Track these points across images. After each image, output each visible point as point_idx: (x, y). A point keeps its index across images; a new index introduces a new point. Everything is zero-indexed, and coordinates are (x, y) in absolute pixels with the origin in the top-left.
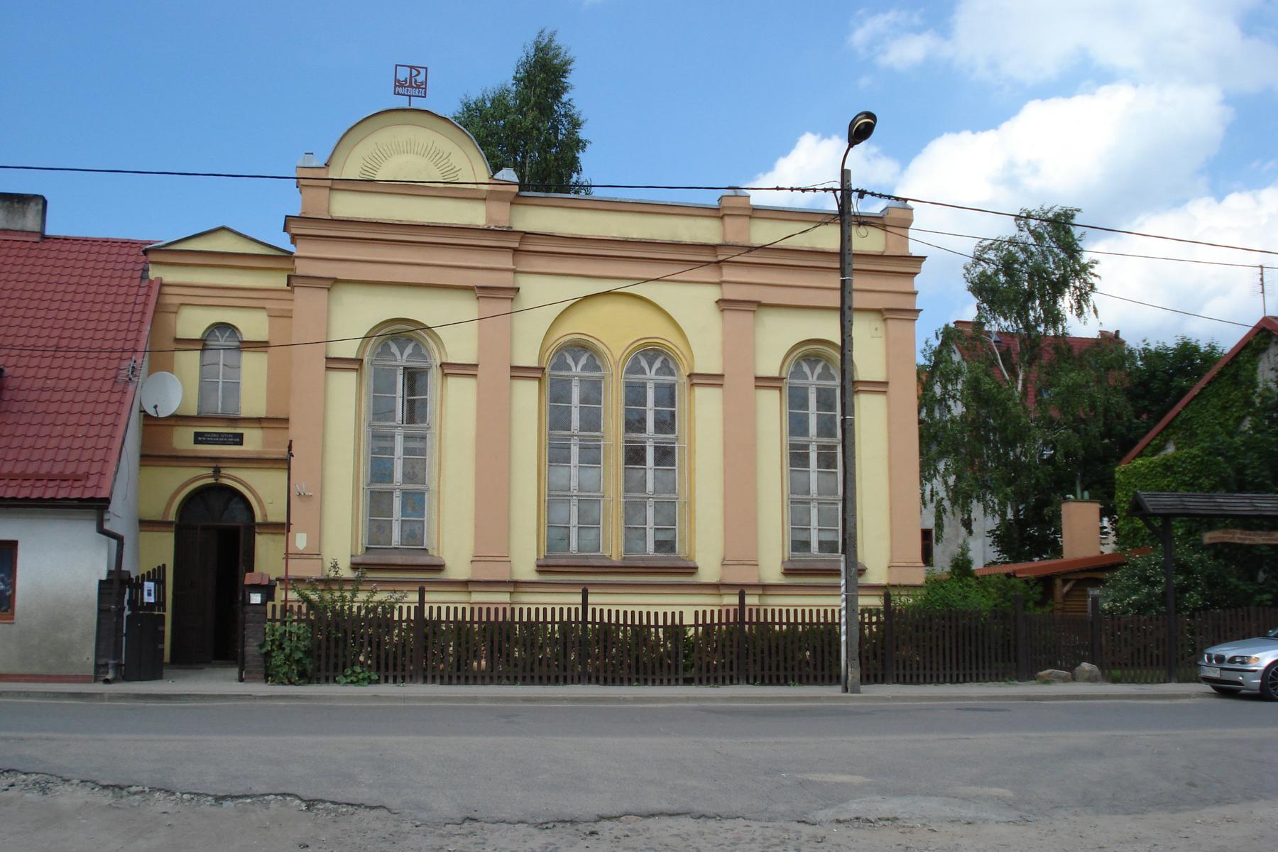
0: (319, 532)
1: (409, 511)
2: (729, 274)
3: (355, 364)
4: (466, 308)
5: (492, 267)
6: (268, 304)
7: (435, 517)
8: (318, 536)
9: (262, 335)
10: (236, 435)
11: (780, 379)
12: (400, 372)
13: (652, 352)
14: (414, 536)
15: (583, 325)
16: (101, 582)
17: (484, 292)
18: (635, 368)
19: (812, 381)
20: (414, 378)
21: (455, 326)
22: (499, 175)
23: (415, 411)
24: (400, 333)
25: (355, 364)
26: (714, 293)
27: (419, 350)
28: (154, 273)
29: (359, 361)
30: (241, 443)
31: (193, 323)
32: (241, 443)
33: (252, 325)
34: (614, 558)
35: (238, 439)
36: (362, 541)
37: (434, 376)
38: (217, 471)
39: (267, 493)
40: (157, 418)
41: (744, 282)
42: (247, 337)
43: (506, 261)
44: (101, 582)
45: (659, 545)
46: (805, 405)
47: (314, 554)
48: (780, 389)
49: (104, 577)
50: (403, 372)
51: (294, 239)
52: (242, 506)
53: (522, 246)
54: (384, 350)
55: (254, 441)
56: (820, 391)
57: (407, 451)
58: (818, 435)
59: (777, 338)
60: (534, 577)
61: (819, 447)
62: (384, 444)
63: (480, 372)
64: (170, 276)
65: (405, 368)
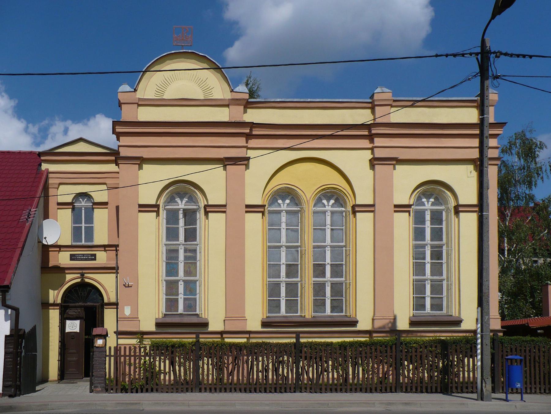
0: (140, 303)
1: (188, 293)
2: (378, 142)
3: (154, 208)
4: (218, 171)
5: (232, 146)
6: (107, 181)
7: (411, 251)
8: (135, 309)
9: (105, 200)
10: (92, 255)
11: (409, 206)
12: (181, 212)
13: (330, 194)
14: (191, 305)
15: (284, 179)
16: (6, 336)
17: (226, 162)
18: (318, 201)
19: (428, 205)
20: (190, 216)
21: (213, 182)
22: (237, 89)
23: (191, 235)
24: (182, 189)
25: (154, 208)
26: (368, 155)
27: (192, 199)
28: (44, 166)
29: (157, 206)
30: (95, 259)
31: (65, 193)
32: (95, 259)
33: (100, 194)
34: (307, 317)
35: (93, 257)
36: (163, 309)
37: (201, 215)
38: (82, 275)
39: (106, 283)
40: (48, 245)
41: (386, 146)
42: (97, 200)
43: (241, 141)
44: (6, 336)
45: (433, 307)
46: (423, 222)
47: (134, 318)
48: (409, 212)
49: (8, 333)
50: (183, 208)
51: (119, 135)
52: (97, 294)
53: (250, 132)
54: (171, 199)
55: (102, 258)
56: (433, 212)
57: (186, 258)
58: (432, 240)
59: (405, 181)
60: (259, 328)
61: (432, 247)
62: (173, 255)
63: (228, 209)
64: (53, 168)
65: (184, 210)
